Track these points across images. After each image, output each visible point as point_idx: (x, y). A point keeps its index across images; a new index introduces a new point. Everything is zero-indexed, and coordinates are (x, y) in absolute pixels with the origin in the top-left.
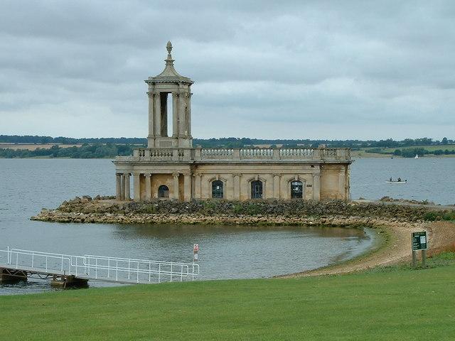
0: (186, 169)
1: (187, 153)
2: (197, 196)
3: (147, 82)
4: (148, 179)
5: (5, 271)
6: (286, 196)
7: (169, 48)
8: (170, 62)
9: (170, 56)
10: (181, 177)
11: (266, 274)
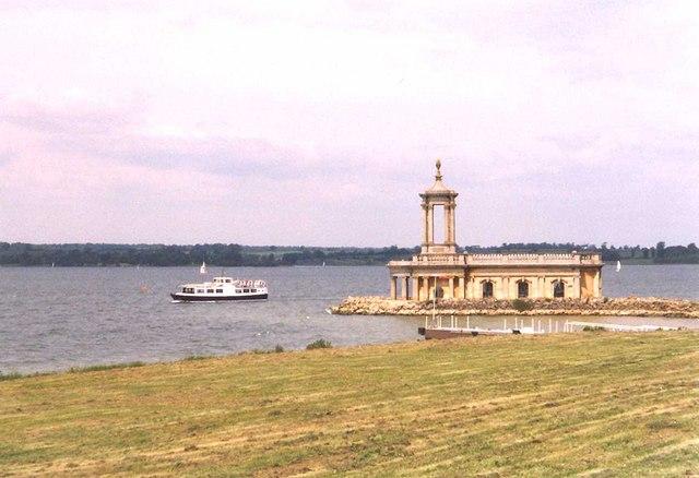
0: (461, 274)
2: (470, 296)
3: (421, 196)
4: (426, 282)
5: (696, 263)
6: (550, 295)
10: (456, 280)
11: (681, 266)
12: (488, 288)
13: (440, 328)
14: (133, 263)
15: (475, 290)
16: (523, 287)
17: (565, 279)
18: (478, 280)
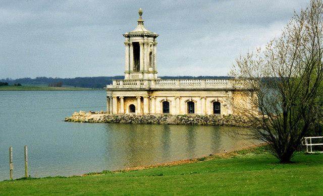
1: (146, 83)
4: (122, 100)
6: (210, 112)
10: (142, 99)
12: (166, 106)
13: (311, 138)
14: (212, 77)
15: (156, 108)
16: (191, 105)
17: (220, 99)
18: (159, 99)
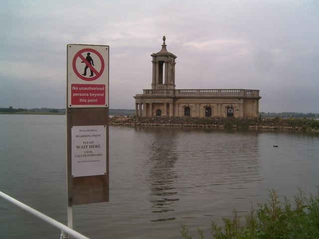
3: (151, 55)
4: (151, 106)
7: (164, 39)
8: (164, 46)
9: (164, 43)
10: (168, 105)
